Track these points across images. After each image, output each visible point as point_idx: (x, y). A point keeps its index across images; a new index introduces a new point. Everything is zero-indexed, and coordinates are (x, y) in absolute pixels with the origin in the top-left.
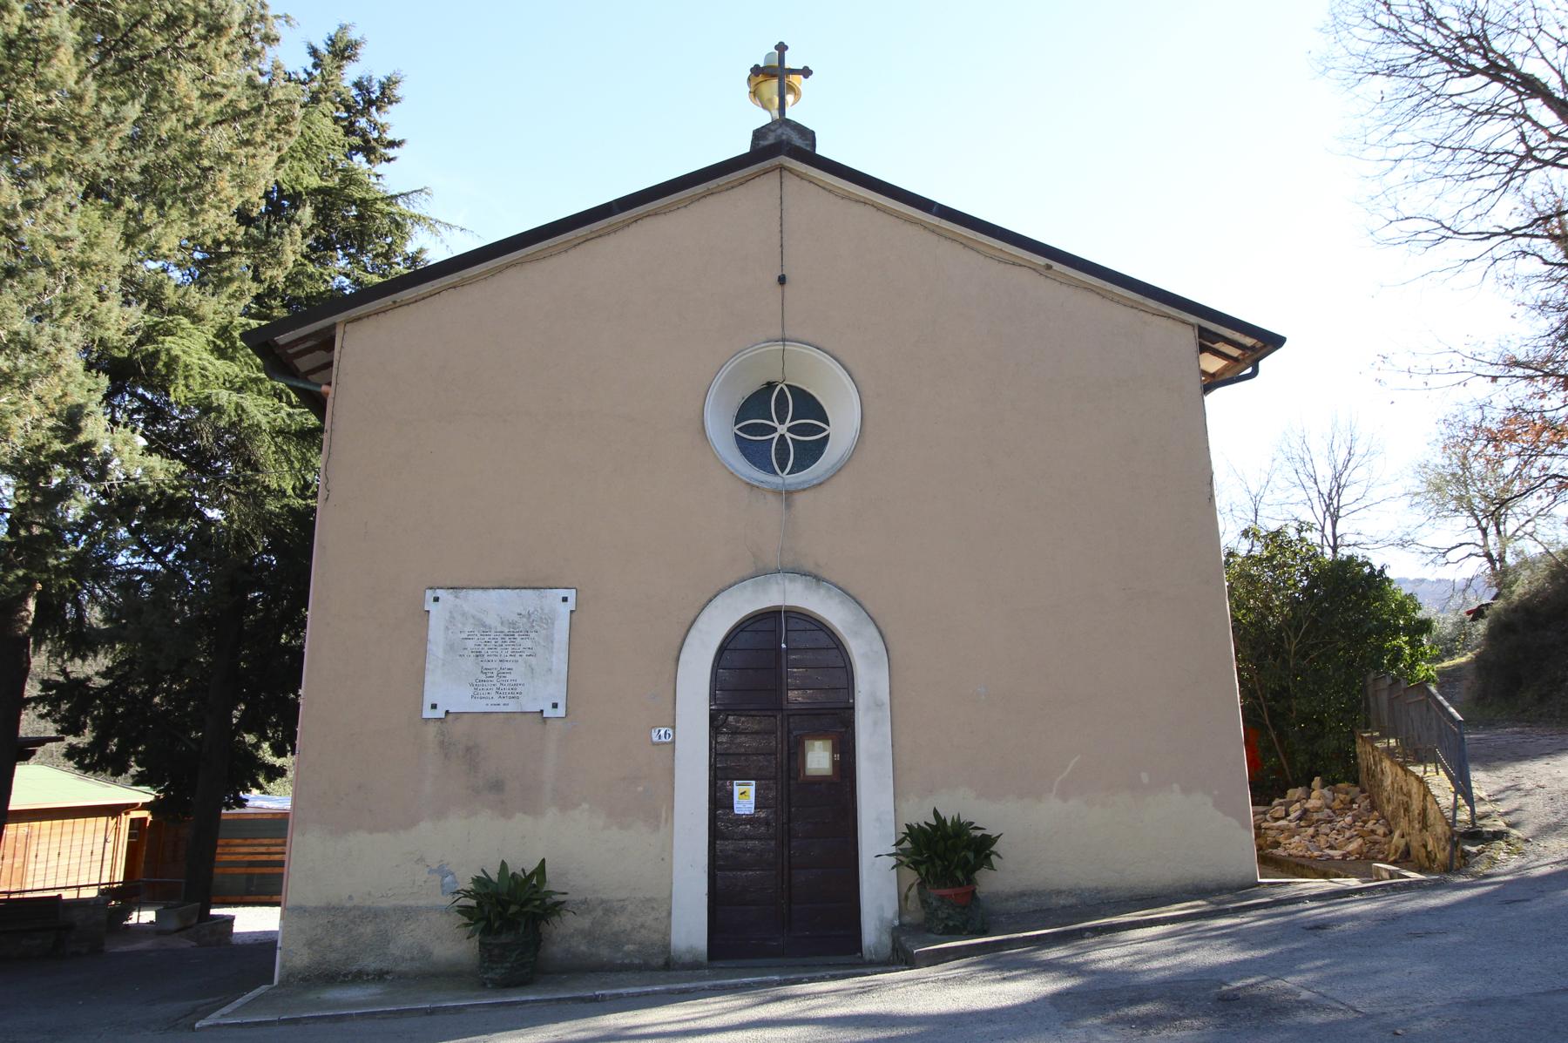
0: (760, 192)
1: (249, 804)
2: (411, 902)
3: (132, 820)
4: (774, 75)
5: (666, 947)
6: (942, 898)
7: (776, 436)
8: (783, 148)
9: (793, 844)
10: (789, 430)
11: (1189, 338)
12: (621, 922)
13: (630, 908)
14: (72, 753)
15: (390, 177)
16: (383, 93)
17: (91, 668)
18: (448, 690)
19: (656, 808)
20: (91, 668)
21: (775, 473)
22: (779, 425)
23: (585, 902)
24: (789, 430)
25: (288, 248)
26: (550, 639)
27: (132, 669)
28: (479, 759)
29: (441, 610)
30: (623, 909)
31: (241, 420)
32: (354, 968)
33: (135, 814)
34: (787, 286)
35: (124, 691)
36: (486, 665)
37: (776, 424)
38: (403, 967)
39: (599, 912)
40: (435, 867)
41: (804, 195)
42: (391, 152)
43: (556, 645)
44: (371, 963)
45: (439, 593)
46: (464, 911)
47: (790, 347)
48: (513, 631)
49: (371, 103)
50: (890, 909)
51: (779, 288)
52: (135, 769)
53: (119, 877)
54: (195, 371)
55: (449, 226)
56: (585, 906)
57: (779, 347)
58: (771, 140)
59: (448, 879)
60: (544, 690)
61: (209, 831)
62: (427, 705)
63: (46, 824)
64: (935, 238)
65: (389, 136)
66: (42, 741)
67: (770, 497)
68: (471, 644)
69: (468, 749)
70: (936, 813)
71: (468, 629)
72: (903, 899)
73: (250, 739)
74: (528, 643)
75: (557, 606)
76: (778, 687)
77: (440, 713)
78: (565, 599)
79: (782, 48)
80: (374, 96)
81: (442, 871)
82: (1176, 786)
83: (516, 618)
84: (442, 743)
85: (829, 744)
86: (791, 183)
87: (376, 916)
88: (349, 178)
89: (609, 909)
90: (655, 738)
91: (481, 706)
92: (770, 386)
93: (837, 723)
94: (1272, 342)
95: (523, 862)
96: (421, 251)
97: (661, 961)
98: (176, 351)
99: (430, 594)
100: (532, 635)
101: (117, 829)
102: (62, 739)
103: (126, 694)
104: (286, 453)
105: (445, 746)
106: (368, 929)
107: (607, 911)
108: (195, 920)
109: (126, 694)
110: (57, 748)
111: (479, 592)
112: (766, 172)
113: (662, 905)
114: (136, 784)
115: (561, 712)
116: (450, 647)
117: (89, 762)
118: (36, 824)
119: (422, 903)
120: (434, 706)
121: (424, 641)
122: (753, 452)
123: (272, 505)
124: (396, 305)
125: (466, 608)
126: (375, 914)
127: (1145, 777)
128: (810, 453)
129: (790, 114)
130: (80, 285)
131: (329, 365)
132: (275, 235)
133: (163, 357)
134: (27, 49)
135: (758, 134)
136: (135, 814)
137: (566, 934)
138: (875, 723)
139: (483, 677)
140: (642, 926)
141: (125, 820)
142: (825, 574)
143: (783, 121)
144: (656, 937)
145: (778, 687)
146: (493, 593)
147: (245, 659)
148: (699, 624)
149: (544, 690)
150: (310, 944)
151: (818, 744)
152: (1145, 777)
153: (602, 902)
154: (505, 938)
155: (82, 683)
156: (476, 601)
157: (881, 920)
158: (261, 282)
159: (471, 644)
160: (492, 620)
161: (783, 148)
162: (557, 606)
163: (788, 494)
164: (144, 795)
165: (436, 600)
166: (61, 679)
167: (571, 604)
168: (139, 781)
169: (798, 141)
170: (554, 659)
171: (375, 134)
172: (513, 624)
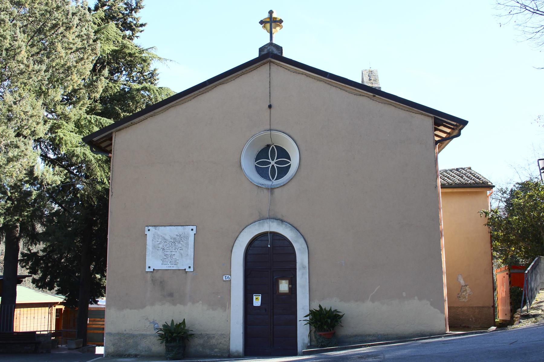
0: (263, 72)
1: (99, 303)
2: (144, 333)
3: (57, 309)
4: (271, 22)
5: (229, 350)
6: (321, 335)
7: (271, 165)
8: (271, 55)
9: (275, 317)
10: (276, 163)
11: (429, 122)
12: (213, 341)
13: (216, 337)
14: (34, 281)
15: (141, 41)
16: (137, 5)
17: (38, 248)
18: (154, 262)
19: (224, 303)
20: (38, 248)
21: (270, 180)
22: (271, 160)
23: (201, 334)
24: (276, 163)
25: (100, 87)
26: (187, 244)
27: (53, 248)
28: (165, 285)
29: (151, 233)
30: (214, 337)
31: (85, 159)
32: (128, 353)
33: (58, 307)
34: (272, 110)
35: (50, 257)
36: (166, 253)
37: (271, 161)
38: (143, 353)
39: (206, 338)
40: (152, 321)
41: (279, 73)
42: (141, 29)
43: (189, 246)
44: (133, 352)
45: (150, 228)
46: (161, 335)
47: (274, 132)
48: (175, 241)
49: (132, 10)
50: (307, 340)
51: (269, 110)
52: (56, 288)
53: (54, 328)
54: (69, 142)
55: (166, 60)
56: (201, 336)
57: (269, 133)
58: (265, 52)
59: (156, 326)
60: (186, 262)
61: (85, 313)
62: (147, 267)
63: (25, 309)
64: (330, 86)
65: (140, 22)
66: (25, 277)
67: (265, 191)
68: (161, 246)
69: (161, 282)
70: (320, 306)
71: (160, 240)
72: (310, 335)
73: (98, 276)
74: (180, 245)
75: (190, 232)
76: (269, 262)
77: (151, 270)
78: (192, 230)
79: (271, 12)
80: (133, 7)
81: (154, 323)
82: (416, 298)
83: (176, 236)
84: (152, 280)
85: (287, 281)
86: (274, 68)
87: (133, 337)
88: (124, 46)
89: (209, 337)
90: (224, 279)
91: (164, 267)
92: (268, 146)
93: (291, 276)
94: (464, 123)
95: (178, 320)
96: (155, 70)
97: (227, 355)
98: (62, 136)
99: (147, 228)
100: (181, 242)
101: (51, 313)
102: (31, 276)
103: (52, 259)
104: (103, 167)
105: (154, 281)
106: (131, 341)
107: (208, 338)
108: (81, 346)
109: (52, 259)
110: (30, 279)
111: (163, 227)
112: (264, 64)
113: (227, 336)
114: (57, 294)
115: (192, 269)
116: (154, 247)
117: (40, 285)
118: (22, 309)
119: (148, 333)
120: (149, 267)
121: (145, 244)
122: (262, 172)
123: (99, 188)
124: (133, 124)
125: (159, 233)
126: (133, 336)
127: (404, 294)
128: (283, 172)
129: (275, 41)
130: (30, 121)
131: (111, 144)
132: (95, 81)
133: (58, 138)
134: (12, 53)
135: (261, 50)
136: (58, 307)
137: (196, 344)
138: (303, 274)
139: (165, 257)
140: (220, 343)
141: (54, 309)
142: (285, 219)
143: (271, 44)
144: (225, 347)
145: (269, 262)
146: (168, 228)
147: (94, 245)
148: (239, 238)
149: (186, 262)
150: (113, 345)
151: (284, 281)
152: (404, 294)
153: (207, 335)
154: (172, 344)
155: (35, 254)
156: (163, 230)
157: (304, 343)
158: (91, 99)
159: (161, 246)
160: (167, 237)
161: (271, 55)
162: (190, 232)
163: (271, 190)
164: (60, 299)
165: (149, 230)
166: (29, 252)
167: (194, 232)
168: (58, 293)
169: (276, 52)
170: (189, 251)
171: (135, 22)
172: (175, 239)
